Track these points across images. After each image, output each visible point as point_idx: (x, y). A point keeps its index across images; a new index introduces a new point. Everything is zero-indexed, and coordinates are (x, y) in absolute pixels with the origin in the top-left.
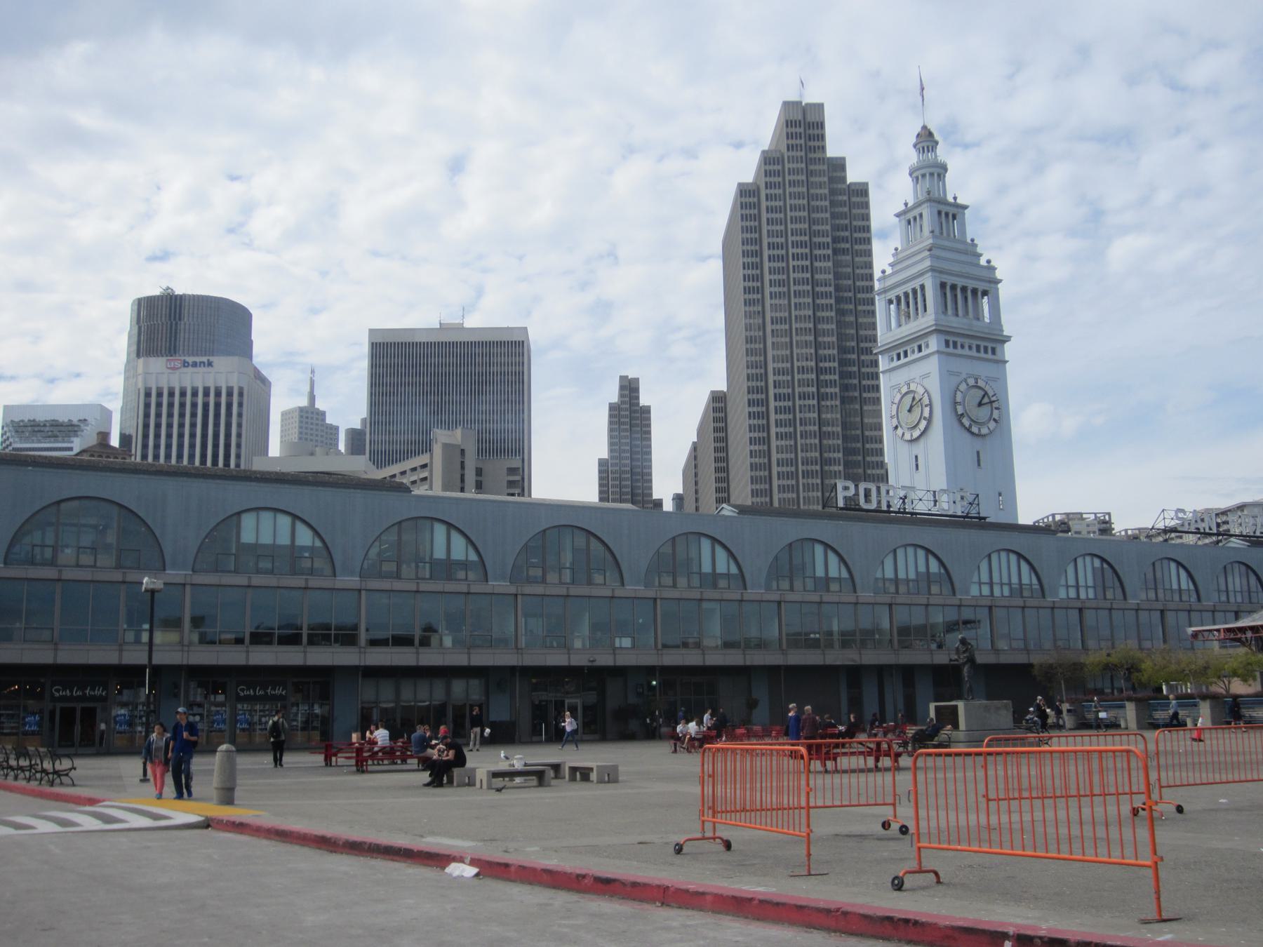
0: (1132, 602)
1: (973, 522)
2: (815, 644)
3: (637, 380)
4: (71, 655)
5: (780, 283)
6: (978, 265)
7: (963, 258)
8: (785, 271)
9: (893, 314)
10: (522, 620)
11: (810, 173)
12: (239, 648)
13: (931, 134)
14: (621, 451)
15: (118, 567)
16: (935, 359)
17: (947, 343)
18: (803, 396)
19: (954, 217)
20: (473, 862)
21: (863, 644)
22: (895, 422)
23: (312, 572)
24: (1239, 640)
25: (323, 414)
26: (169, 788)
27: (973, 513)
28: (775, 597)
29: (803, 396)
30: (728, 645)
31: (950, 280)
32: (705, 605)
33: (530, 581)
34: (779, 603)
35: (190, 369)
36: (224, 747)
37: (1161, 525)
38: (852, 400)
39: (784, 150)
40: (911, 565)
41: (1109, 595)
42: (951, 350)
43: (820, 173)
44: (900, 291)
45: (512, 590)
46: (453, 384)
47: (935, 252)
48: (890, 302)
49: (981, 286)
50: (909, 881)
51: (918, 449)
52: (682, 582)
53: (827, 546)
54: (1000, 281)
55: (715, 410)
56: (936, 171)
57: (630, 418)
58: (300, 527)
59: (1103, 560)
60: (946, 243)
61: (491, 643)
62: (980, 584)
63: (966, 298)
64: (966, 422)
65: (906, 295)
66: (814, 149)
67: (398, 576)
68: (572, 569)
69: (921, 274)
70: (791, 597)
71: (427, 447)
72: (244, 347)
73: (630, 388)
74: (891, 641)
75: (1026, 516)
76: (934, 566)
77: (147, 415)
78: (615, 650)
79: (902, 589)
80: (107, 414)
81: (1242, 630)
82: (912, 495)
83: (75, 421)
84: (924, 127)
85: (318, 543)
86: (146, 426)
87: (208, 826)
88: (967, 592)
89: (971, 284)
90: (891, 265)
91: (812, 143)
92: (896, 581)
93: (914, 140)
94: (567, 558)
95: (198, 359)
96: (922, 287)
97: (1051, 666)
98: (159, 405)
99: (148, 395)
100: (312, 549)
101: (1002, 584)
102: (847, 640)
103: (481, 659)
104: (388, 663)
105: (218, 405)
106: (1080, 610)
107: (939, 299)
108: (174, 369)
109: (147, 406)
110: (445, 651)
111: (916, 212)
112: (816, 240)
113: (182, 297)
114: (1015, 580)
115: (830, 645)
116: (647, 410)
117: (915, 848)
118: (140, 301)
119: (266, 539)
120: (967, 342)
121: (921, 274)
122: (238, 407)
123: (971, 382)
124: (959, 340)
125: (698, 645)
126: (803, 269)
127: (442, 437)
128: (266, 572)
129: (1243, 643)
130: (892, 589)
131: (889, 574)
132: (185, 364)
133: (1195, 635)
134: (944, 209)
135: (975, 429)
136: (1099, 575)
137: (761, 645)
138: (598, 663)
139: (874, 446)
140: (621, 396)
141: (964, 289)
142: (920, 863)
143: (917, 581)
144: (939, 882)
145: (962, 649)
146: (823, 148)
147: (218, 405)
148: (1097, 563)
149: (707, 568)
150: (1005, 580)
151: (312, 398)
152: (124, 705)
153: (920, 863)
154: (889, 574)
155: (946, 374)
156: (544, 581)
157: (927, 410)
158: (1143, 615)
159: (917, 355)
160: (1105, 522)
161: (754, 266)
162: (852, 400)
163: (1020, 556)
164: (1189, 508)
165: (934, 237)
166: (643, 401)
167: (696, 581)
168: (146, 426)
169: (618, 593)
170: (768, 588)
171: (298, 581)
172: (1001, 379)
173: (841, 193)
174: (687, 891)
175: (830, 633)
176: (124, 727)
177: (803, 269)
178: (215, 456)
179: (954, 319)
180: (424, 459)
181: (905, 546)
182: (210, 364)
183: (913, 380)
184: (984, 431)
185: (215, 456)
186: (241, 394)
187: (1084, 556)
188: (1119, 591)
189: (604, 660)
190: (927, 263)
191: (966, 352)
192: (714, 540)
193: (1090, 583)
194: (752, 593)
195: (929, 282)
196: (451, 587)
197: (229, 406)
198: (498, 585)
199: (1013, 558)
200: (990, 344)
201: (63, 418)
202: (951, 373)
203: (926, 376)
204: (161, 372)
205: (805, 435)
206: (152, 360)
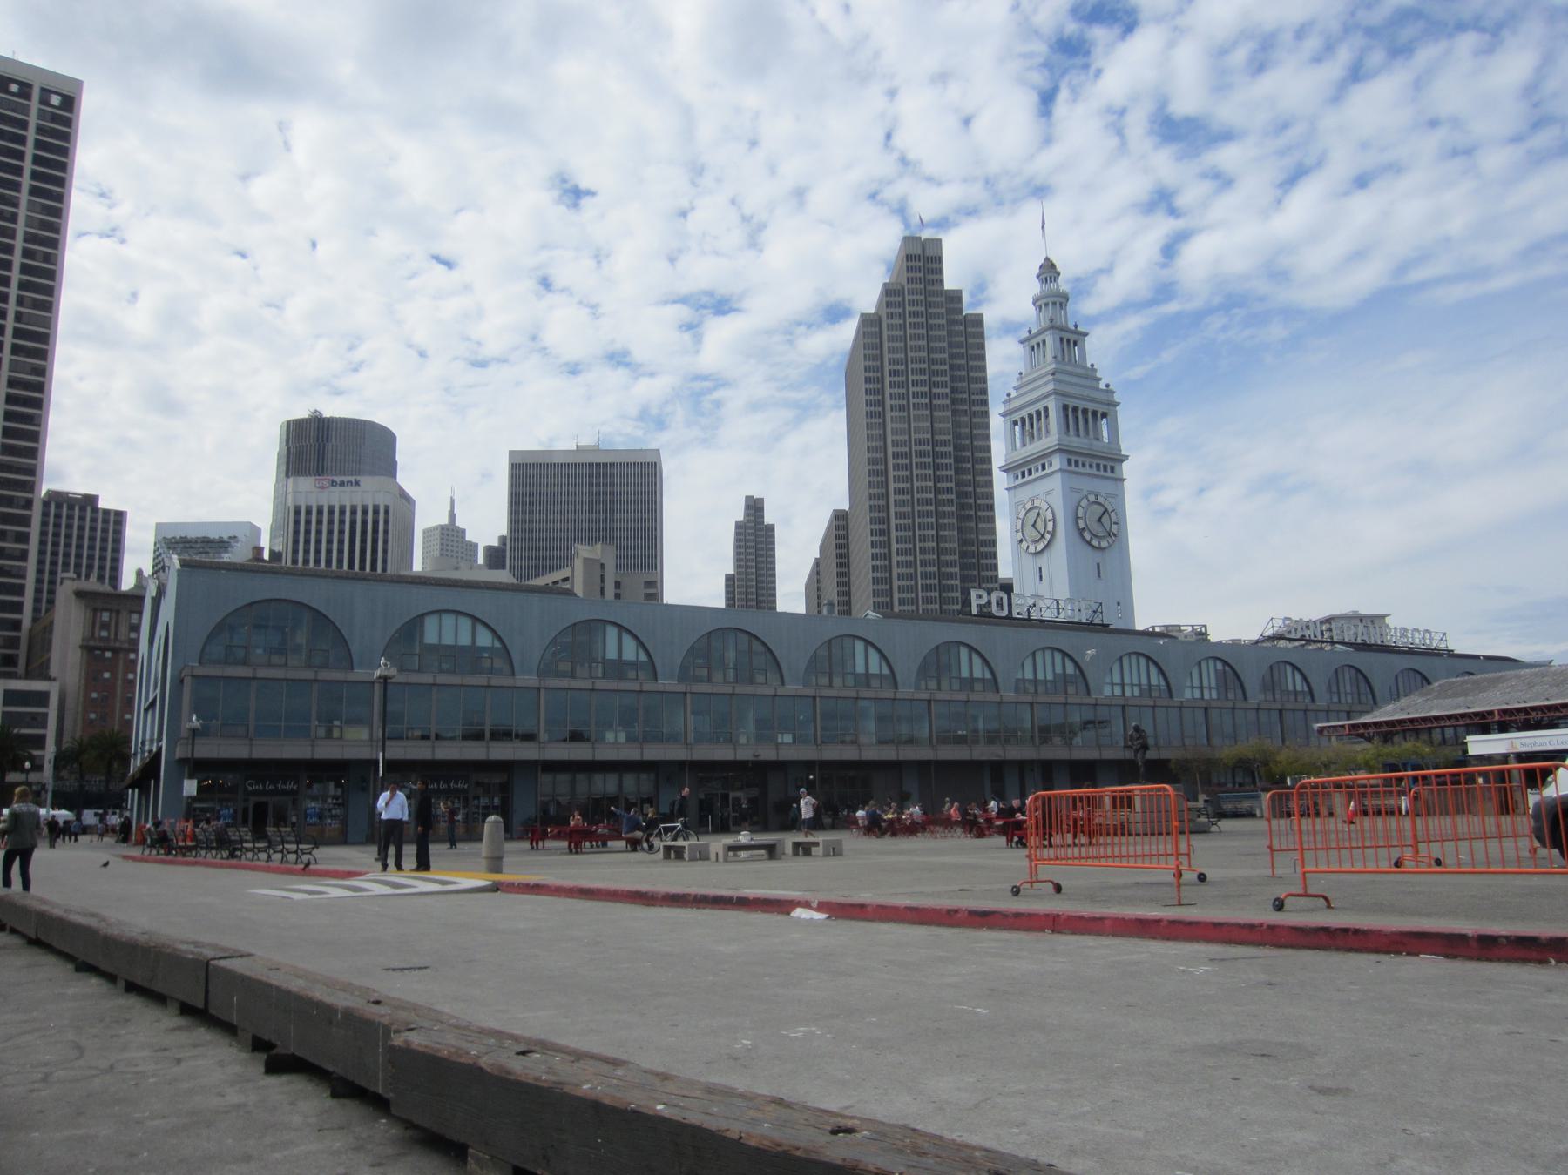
0: (1253, 702)
1: (1095, 627)
2: (961, 740)
3: (762, 500)
4: (267, 750)
5: (901, 408)
6: (1098, 389)
7: (1087, 383)
8: (905, 396)
9: (1018, 434)
10: (691, 718)
11: (929, 305)
12: (427, 743)
13: (1053, 266)
14: (747, 567)
15: (309, 667)
16: (1058, 476)
17: (1069, 461)
18: (922, 514)
19: (1075, 344)
20: (822, 907)
21: (1007, 741)
22: (1020, 536)
23: (491, 671)
24: (1362, 736)
25: (464, 531)
26: (410, 861)
27: (1097, 620)
28: (926, 696)
29: (922, 514)
30: (881, 742)
31: (1071, 403)
32: (862, 703)
33: (699, 680)
34: (929, 701)
35: (338, 489)
36: (492, 818)
37: (1269, 633)
38: (968, 518)
39: (904, 282)
40: (1049, 667)
41: (1231, 696)
42: (1073, 468)
43: (940, 305)
44: (1024, 413)
45: (681, 688)
46: (588, 505)
47: (1058, 376)
48: (1015, 423)
49: (1101, 409)
50: (1289, 902)
51: (1043, 561)
52: (837, 681)
53: (971, 649)
54: (1118, 404)
55: (837, 528)
56: (1058, 300)
57: (755, 539)
58: (481, 629)
59: (1225, 663)
60: (1069, 368)
61: (659, 738)
62: (1113, 684)
63: (1086, 421)
64: (1087, 535)
65: (1031, 416)
66: (932, 282)
67: (573, 676)
68: (736, 669)
69: (1045, 397)
70: (940, 696)
71: (568, 560)
72: (390, 468)
73: (755, 507)
74: (1032, 738)
75: (1140, 625)
76: (1070, 669)
77: (296, 532)
78: (777, 746)
79: (1041, 689)
80: (256, 531)
81: (1365, 725)
82: (1041, 604)
83: (226, 538)
84: (1047, 259)
85: (497, 644)
86: (296, 542)
87: (497, 890)
88: (1101, 692)
89: (1091, 407)
90: (1016, 389)
91: (930, 277)
92: (1035, 681)
93: (1037, 271)
94: (731, 655)
95: (345, 479)
96: (1046, 409)
97: (1187, 761)
98: (308, 522)
99: (297, 512)
100: (490, 649)
101: (1132, 685)
102: (992, 738)
103: (653, 753)
104: (566, 757)
105: (364, 523)
106: (1206, 709)
107: (1062, 420)
108: (323, 488)
109: (297, 523)
110: (615, 745)
111: (1039, 339)
112: (934, 367)
113: (330, 420)
114: (1144, 681)
115: (976, 742)
116: (771, 528)
117: (1299, 875)
118: (288, 423)
119: (448, 640)
120: (1088, 461)
121: (1045, 397)
122: (379, 527)
123: (1092, 498)
124: (1081, 459)
125: (854, 742)
126: (922, 395)
127: (583, 551)
128: (448, 671)
129: (1369, 740)
130: (1032, 689)
131: (1029, 675)
132: (333, 483)
133: (1321, 730)
134: (1066, 336)
135: (1095, 543)
136: (1222, 678)
137: (911, 741)
138: (762, 758)
139: (989, 561)
140: (747, 515)
141: (1085, 411)
142: (1305, 887)
143: (1054, 682)
144: (1329, 907)
145: (1136, 735)
146: (941, 281)
147: (364, 523)
148: (1220, 666)
149: (860, 669)
150: (1135, 681)
151: (452, 516)
152: (314, 798)
153: (1305, 887)
154: (1029, 675)
155: (1069, 491)
156: (709, 680)
157: (1050, 525)
158: (1263, 717)
159: (1041, 473)
160: (1201, 634)
161: (875, 392)
162: (968, 518)
163: (1148, 658)
164: (1295, 618)
165: (1057, 362)
166: (768, 520)
167: (850, 680)
168: (296, 542)
169: (780, 692)
170: (917, 688)
171: (481, 680)
172: (1119, 496)
173: (957, 322)
174: (1082, 918)
175: (976, 731)
176: (314, 820)
177: (922, 395)
178: (374, 561)
179: (1075, 439)
180: (566, 572)
181: (1043, 649)
182: (357, 483)
183: (1037, 496)
184: (1104, 544)
185: (374, 561)
186: (387, 512)
187: (1207, 659)
188: (1239, 692)
189: (768, 754)
190: (1051, 387)
191: (1087, 470)
192: (867, 642)
193: (1213, 684)
194: (905, 691)
195: (1052, 405)
196: (624, 685)
197: (376, 523)
198: (666, 683)
199: (1143, 661)
200: (1109, 463)
201: (214, 535)
202: (1073, 490)
203: (1050, 492)
204: (308, 490)
205: (923, 551)
206: (301, 479)
